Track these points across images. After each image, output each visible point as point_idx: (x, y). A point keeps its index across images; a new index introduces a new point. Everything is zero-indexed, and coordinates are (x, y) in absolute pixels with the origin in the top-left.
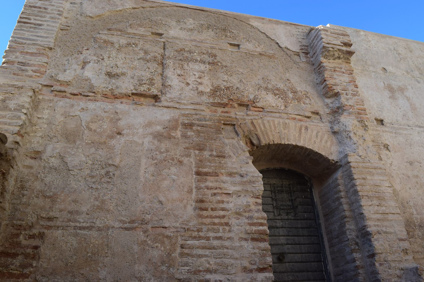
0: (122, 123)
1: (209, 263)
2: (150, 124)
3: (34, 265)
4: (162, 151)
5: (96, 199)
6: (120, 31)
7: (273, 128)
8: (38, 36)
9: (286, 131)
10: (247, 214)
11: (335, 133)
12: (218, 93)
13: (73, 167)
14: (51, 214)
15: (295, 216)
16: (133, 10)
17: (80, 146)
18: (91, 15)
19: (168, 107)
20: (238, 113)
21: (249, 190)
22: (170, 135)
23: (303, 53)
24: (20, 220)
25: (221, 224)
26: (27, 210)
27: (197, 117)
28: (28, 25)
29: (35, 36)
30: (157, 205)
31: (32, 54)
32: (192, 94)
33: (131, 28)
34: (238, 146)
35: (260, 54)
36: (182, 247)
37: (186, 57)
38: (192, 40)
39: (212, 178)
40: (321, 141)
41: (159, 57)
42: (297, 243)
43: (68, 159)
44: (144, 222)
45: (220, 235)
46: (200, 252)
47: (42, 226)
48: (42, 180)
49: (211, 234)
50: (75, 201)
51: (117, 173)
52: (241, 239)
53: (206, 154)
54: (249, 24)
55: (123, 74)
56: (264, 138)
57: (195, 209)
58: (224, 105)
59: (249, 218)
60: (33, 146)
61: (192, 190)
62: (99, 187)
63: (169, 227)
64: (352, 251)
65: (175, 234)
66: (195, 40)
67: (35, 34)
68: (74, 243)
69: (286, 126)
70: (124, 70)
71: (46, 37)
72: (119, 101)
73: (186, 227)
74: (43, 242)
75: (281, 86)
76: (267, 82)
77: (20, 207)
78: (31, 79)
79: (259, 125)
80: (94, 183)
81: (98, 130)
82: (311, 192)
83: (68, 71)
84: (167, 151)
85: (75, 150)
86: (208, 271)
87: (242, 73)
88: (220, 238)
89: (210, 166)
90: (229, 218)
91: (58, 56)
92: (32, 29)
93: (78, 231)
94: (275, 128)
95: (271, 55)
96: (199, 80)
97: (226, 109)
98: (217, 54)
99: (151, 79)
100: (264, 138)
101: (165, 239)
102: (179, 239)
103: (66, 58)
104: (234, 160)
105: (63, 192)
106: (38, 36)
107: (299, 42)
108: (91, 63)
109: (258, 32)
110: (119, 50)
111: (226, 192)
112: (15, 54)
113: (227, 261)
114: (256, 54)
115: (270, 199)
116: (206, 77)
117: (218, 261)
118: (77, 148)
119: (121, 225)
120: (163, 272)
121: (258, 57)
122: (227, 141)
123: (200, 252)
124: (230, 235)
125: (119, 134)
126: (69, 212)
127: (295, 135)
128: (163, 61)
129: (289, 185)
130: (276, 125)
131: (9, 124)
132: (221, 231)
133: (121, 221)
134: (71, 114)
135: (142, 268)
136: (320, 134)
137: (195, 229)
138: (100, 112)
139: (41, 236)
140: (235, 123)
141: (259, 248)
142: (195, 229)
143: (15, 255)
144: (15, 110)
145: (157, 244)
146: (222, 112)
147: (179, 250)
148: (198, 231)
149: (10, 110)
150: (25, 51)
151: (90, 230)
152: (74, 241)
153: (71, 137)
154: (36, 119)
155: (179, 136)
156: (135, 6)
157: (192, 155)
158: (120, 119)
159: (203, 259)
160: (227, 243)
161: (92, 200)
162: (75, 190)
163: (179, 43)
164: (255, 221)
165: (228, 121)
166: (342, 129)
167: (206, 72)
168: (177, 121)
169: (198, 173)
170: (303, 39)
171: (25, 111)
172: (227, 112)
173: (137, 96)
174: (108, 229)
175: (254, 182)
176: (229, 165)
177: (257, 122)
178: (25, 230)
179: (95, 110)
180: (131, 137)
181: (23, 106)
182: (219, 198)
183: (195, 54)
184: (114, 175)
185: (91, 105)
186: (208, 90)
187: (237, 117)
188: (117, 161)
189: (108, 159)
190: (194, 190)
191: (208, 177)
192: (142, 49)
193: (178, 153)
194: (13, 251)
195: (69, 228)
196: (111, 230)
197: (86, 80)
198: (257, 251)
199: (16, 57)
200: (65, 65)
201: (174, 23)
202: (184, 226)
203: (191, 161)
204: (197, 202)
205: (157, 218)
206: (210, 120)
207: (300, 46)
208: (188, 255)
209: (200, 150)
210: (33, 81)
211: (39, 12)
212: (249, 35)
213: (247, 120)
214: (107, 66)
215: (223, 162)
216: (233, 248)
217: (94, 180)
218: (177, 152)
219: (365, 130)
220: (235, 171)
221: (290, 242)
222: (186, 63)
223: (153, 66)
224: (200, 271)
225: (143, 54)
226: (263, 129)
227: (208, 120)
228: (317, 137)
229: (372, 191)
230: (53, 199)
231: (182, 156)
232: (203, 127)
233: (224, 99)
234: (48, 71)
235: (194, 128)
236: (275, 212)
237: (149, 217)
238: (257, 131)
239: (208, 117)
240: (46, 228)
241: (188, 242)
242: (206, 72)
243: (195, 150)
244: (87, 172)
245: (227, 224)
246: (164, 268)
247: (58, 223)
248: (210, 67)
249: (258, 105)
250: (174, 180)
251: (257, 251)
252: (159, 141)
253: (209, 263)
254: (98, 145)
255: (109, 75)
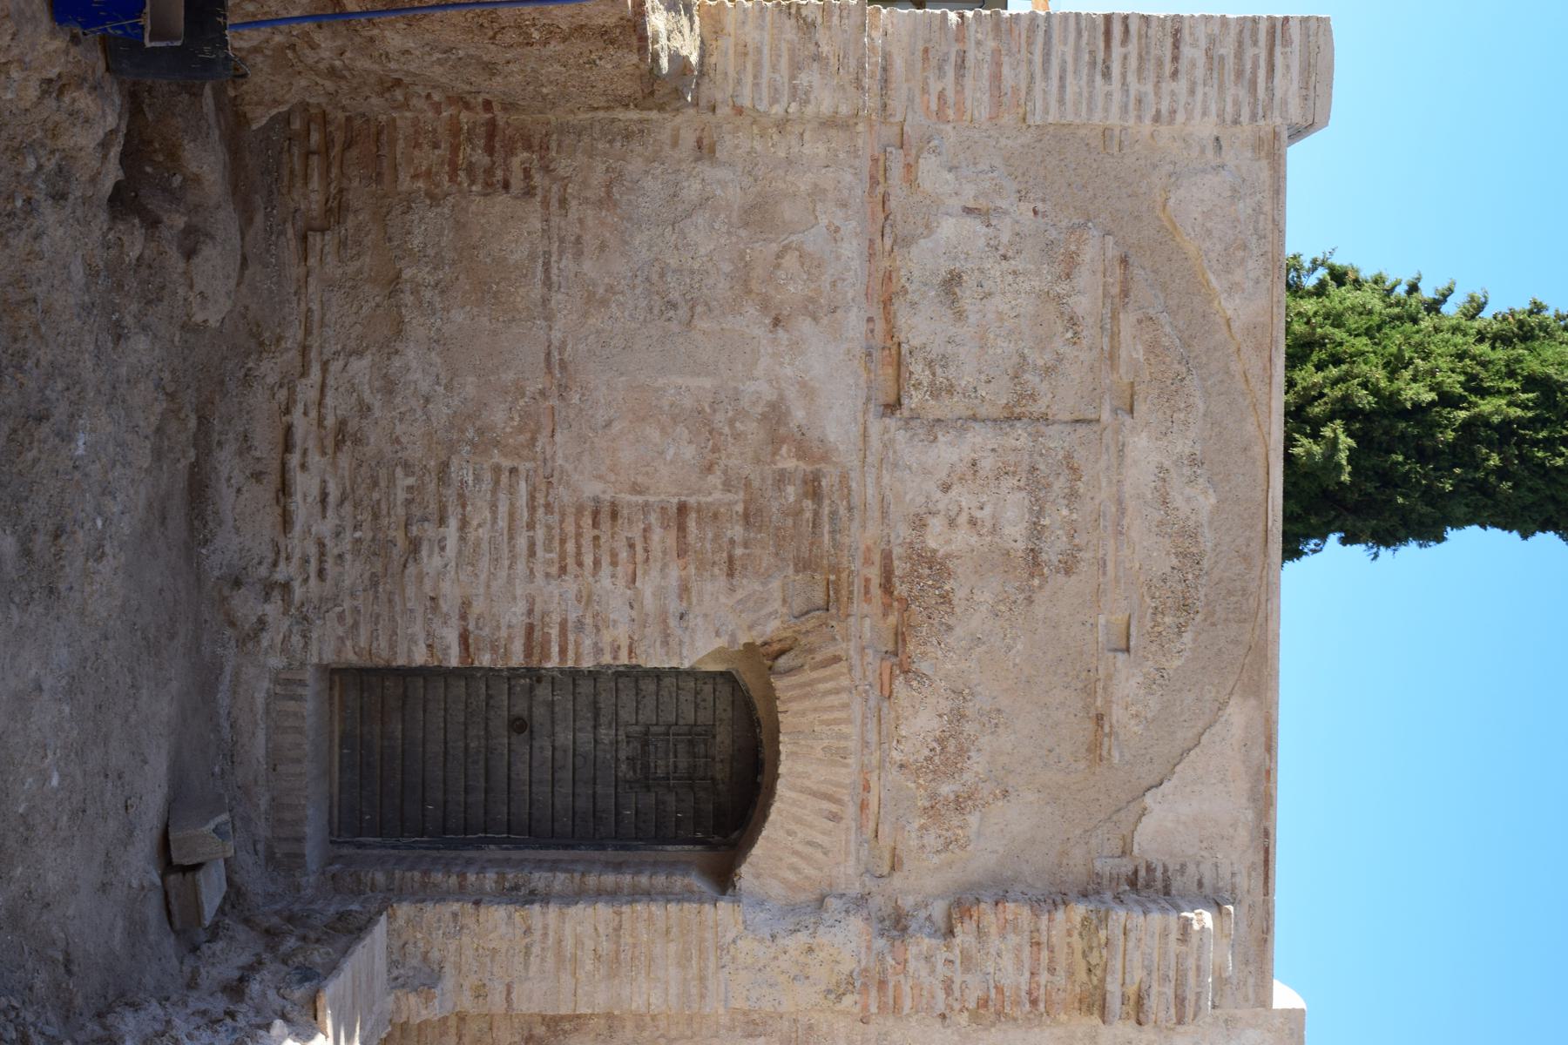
0: (805, 326)
1: (480, 525)
2: (808, 391)
3: (474, 188)
4: (738, 424)
5: (610, 289)
6: (1125, 293)
7: (825, 717)
8: (1062, 79)
9: (819, 753)
10: (588, 620)
11: (821, 901)
12: (927, 571)
13: (682, 231)
14: (574, 203)
15: (627, 781)
16: (1222, 321)
17: (734, 239)
18: (1172, 202)
19: (865, 435)
20: (866, 623)
21: (648, 631)
22: (783, 442)
23: (1136, 872)
24: (559, 145)
25: (563, 557)
26: (579, 155)
27: (842, 511)
28: (1101, 45)
29: (1063, 71)
30: (601, 416)
31: (997, 77)
32: (912, 500)
33: (1140, 322)
34: (764, 612)
35: (1099, 718)
36: (513, 471)
37: (1049, 485)
38: (1120, 502)
39: (671, 539)
40: (796, 853)
41: (1037, 408)
42: (557, 776)
43: (700, 219)
44: (563, 389)
45: (540, 552)
46: (503, 509)
47: (549, 190)
48: (647, 172)
49: (540, 533)
50: (603, 247)
51: (674, 327)
52: (531, 601)
53: (737, 531)
54: (1231, 694)
55: (960, 315)
56: (793, 687)
57: (596, 500)
58: (887, 587)
59: (580, 625)
60: (728, 137)
61: (640, 493)
62: (638, 291)
63: (554, 443)
64: (502, 877)
65: (540, 456)
66: (1122, 511)
67: (1070, 68)
68: (516, 256)
69: (837, 756)
70: (973, 319)
71: (1062, 101)
72: (876, 311)
73: (554, 480)
74: (516, 198)
75: (977, 765)
76: (985, 719)
77: (586, 139)
78: (918, 92)
79: (831, 678)
80: (648, 279)
81: (781, 273)
82: (695, 842)
83: (950, 177)
84: (737, 436)
85: (724, 229)
86: (464, 524)
87: (1009, 648)
88: (532, 553)
89: (702, 540)
90: (576, 576)
91: (1003, 141)
92: (1086, 57)
93: (540, 261)
94: (828, 723)
95: (1104, 753)
96: (963, 519)
97: (876, 591)
98: (1074, 577)
99: (950, 390)
100: (793, 687)
101: (528, 435)
102: (529, 465)
103: (998, 162)
104: (723, 599)
105: (622, 219)
106: (1062, 79)
107: (1183, 866)
108: (985, 230)
109: (1200, 724)
110: (1045, 296)
111: (639, 573)
112: (990, 36)
113: (484, 563)
114: (1099, 703)
115: (672, 719)
116: (975, 538)
117: (485, 546)
118: (729, 233)
119: (556, 343)
120: (462, 431)
121: (1086, 708)
122: (775, 584)
123: (503, 509)
124: (539, 575)
125: (777, 322)
126: (579, 238)
127: (809, 778)
128: (1025, 420)
129: (713, 779)
130: (836, 728)
131: (756, 85)
132: (549, 556)
133: (564, 343)
134: (819, 206)
135: (470, 390)
136: (819, 855)
137: (550, 499)
138: (831, 271)
139: (529, 192)
140: (833, 611)
141: (510, 638)
142: (550, 499)
143: (490, 150)
144: (795, 87)
145: (517, 419)
146: (867, 580)
147: (506, 463)
148: (548, 506)
149: (793, 77)
150: (1005, 59)
151: (544, 284)
152: (519, 254)
153: (758, 214)
154: (798, 129)
155: (780, 465)
156: (1235, 326)
157: (730, 497)
158: (815, 319)
159: (487, 514)
160: (521, 567)
161: (606, 280)
162: (627, 243)
163: (1102, 464)
164: (571, 637)
165: (837, 592)
166: (825, 916)
167: (997, 539)
168: (825, 458)
169: (682, 509)
170: (1200, 884)
171: (793, 108)
172: (867, 592)
173: (892, 355)
174: (547, 319)
175: (665, 643)
176: (709, 587)
177: (842, 674)
178: (542, 158)
179: (838, 258)
180: (770, 350)
181: (807, 102)
182: (624, 555)
183: (1065, 512)
184: (669, 320)
185: (851, 249)
186: (932, 544)
187: (852, 620)
188: (703, 324)
189: (706, 304)
190: (640, 499)
191: (674, 532)
192: (1060, 358)
193: (733, 462)
194: (497, 146)
195: (546, 242)
196: (544, 324)
197: (927, 226)
198: (504, 633)
199: (979, 43)
200: (975, 164)
201: (1183, 446)
202: (556, 474)
203: (714, 494)
204: (613, 504)
205: (572, 416)
206: (836, 545)
207: (1166, 870)
208: (497, 482)
209: (746, 516)
210: (911, 100)
211: (1160, 63)
212: (1180, 690)
213: (844, 645)
214: (981, 270)
215: (716, 571)
216: (510, 580)
217: (655, 277)
218: (736, 459)
219: (829, 991)
220: (694, 600)
221: (558, 755)
222: (1022, 484)
223: (998, 396)
224: (464, 506)
225: (1040, 362)
226: (822, 687)
227: (834, 539)
228: (810, 843)
229: (635, 945)
230: (607, 201)
231: (725, 472)
232: (814, 526)
233: (911, 590)
234: (949, 128)
235: (808, 504)
236: (637, 728)
237: (575, 399)
238: (814, 668)
239: (846, 540)
240: (545, 197)
241: (523, 484)
242: (997, 539)
243: (745, 502)
244: (673, 263)
245: (563, 570)
246: (470, 434)
247: (555, 220)
248: (1020, 554)
249: (899, 682)
250: (661, 453)
251: (504, 633)
252: (764, 416)
253: (480, 525)
254: (743, 278)
255: (952, 282)
